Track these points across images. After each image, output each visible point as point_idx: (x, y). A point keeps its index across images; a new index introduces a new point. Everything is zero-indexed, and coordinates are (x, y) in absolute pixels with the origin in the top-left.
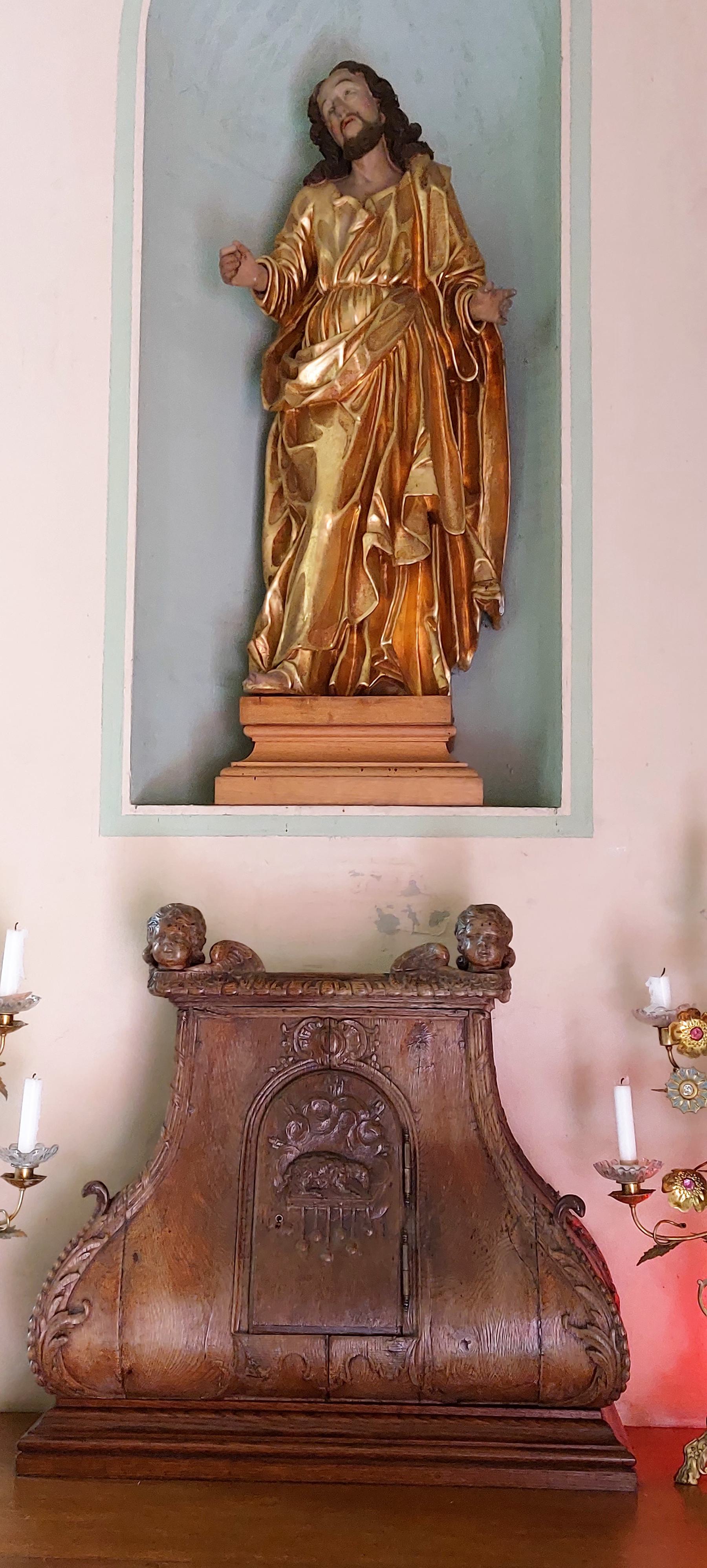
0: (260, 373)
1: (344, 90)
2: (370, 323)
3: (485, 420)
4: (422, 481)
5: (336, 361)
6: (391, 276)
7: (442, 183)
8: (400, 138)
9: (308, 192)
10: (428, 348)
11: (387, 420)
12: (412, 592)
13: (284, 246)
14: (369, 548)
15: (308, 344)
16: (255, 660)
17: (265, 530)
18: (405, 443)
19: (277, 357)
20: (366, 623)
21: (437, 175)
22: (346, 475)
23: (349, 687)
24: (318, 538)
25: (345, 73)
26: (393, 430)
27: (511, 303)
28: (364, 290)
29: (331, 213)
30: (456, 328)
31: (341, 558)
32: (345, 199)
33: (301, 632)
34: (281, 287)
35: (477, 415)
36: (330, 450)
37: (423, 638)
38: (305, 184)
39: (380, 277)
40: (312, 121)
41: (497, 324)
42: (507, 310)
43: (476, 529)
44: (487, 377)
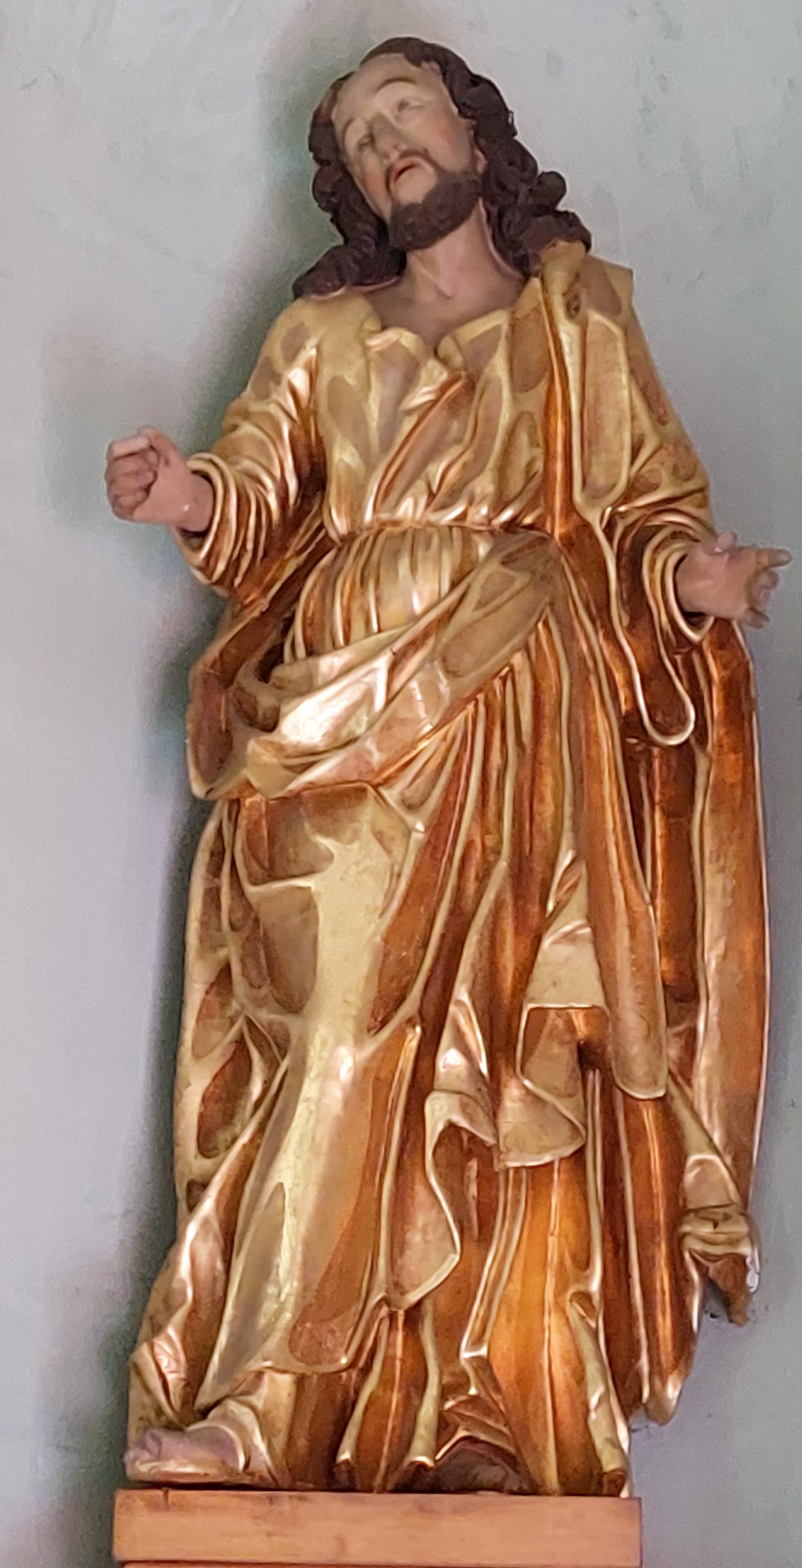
0: (185, 711)
1: (396, 99)
2: (451, 613)
3: (707, 831)
4: (566, 976)
5: (368, 696)
6: (499, 505)
7: (613, 306)
8: (518, 206)
9: (304, 312)
10: (582, 672)
11: (486, 832)
12: (537, 1235)
13: (247, 428)
14: (440, 1127)
15: (301, 651)
16: (148, 1391)
17: (181, 1071)
18: (529, 881)
19: (225, 675)
20: (428, 1306)
21: (601, 288)
22: (386, 955)
23: (383, 1464)
24: (319, 1102)
25: (398, 64)
26: (498, 853)
27: (774, 581)
28: (435, 541)
29: (360, 363)
30: (644, 623)
31: (371, 1153)
32: (391, 335)
33: (271, 1327)
34: (242, 522)
35: (690, 821)
36: (349, 897)
37: (564, 1342)
38: (299, 291)
39: (472, 511)
40: (317, 159)
41: (740, 624)
42: (767, 595)
43: (689, 1082)
44: (714, 733)
